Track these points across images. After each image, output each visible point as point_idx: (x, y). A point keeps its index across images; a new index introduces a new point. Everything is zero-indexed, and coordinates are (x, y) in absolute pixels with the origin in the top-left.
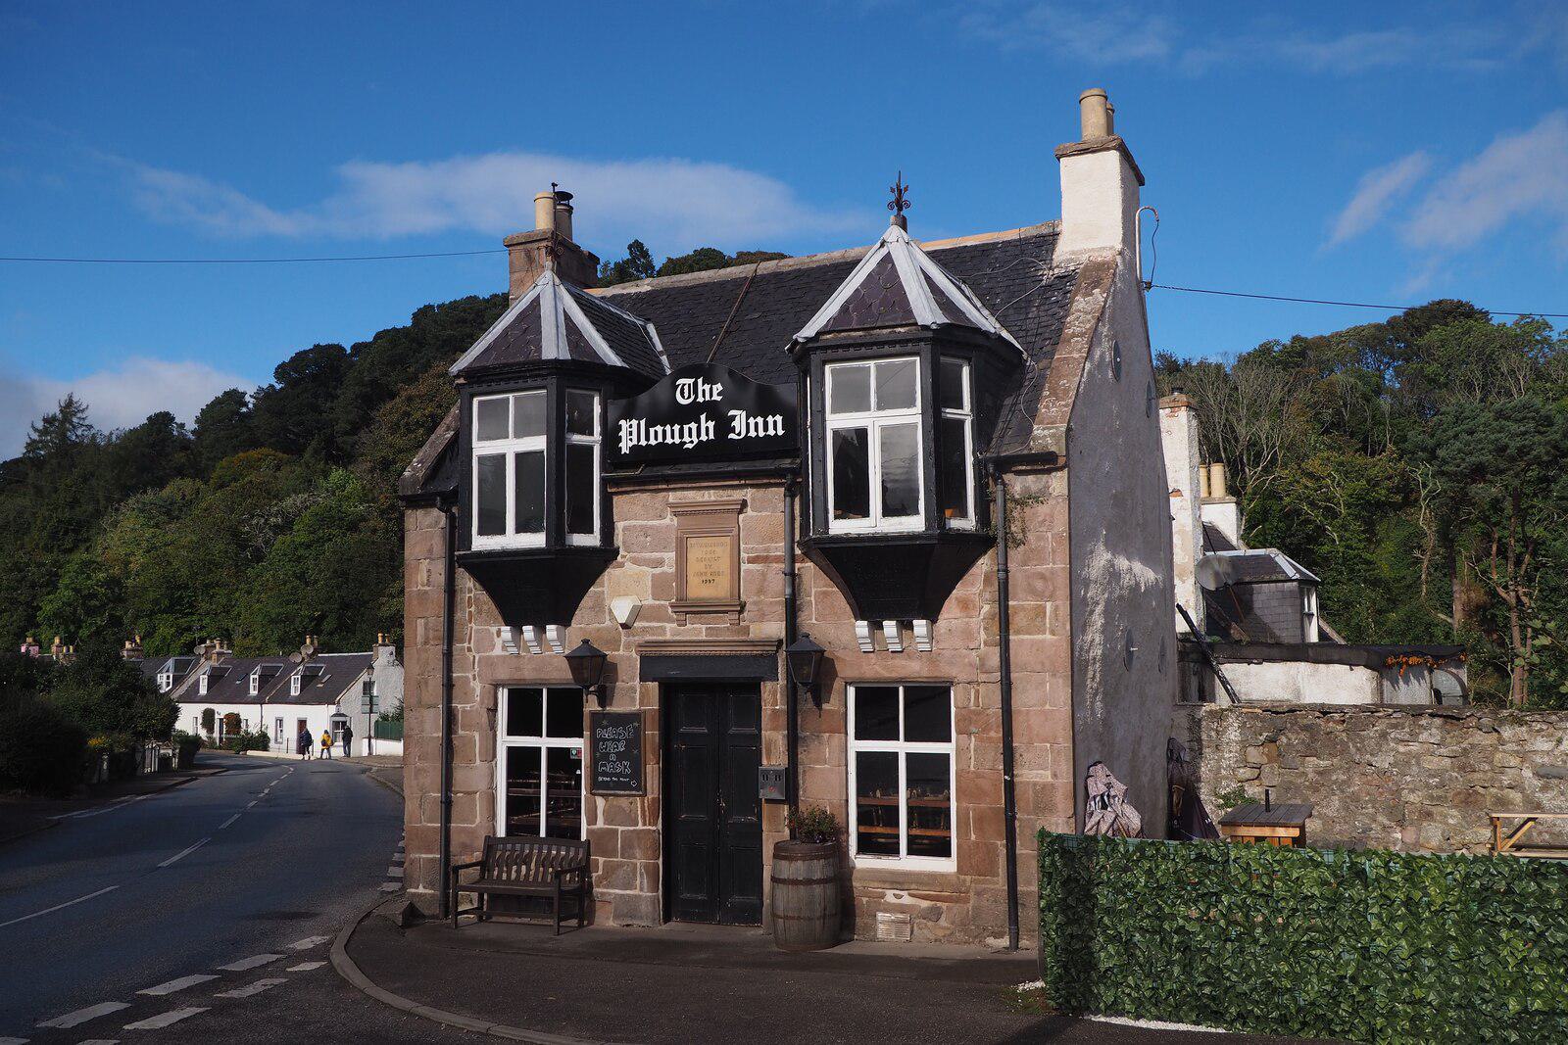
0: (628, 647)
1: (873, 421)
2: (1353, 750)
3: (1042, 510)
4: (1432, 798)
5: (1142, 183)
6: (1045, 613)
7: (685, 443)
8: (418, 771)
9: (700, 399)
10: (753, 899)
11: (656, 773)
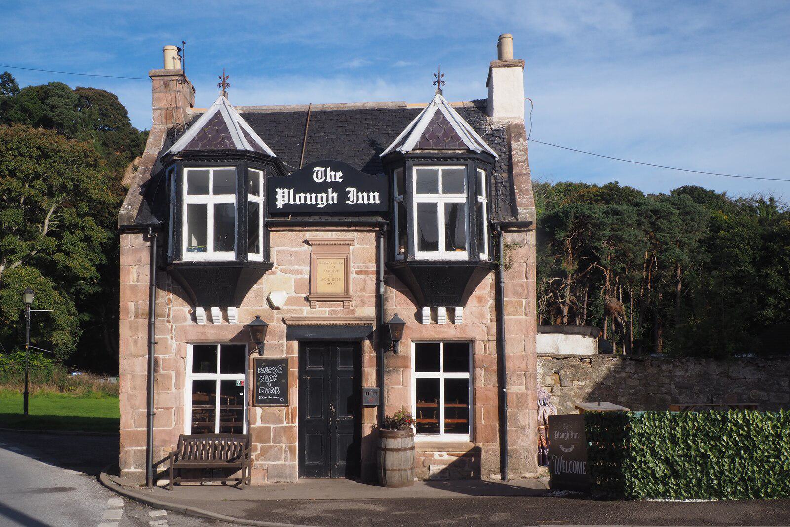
3: (522, 251)
6: (523, 305)
7: (319, 204)
9: (329, 180)
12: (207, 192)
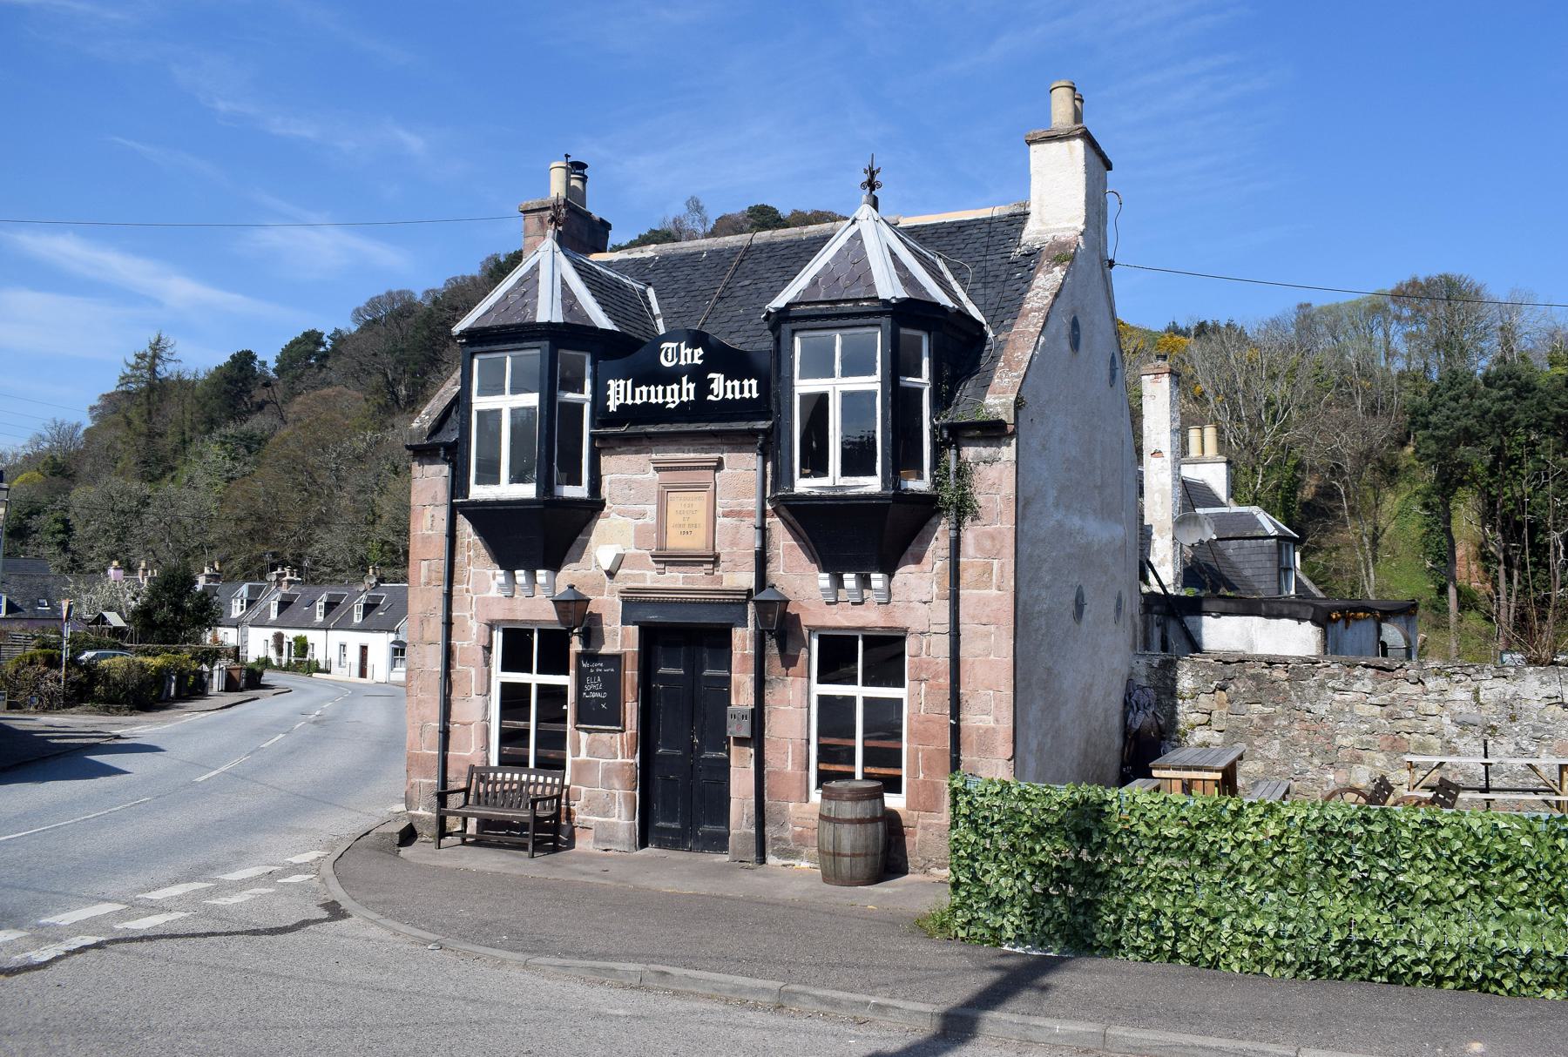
0: (611, 593)
1: (836, 387)
2: (1294, 698)
4: (1362, 742)
5: (1108, 166)
7: (667, 403)
8: (420, 702)
9: (683, 362)
10: (722, 829)
11: (635, 711)
12: (502, 392)
